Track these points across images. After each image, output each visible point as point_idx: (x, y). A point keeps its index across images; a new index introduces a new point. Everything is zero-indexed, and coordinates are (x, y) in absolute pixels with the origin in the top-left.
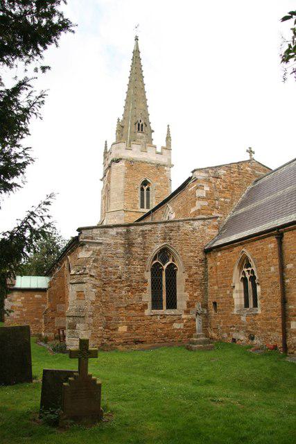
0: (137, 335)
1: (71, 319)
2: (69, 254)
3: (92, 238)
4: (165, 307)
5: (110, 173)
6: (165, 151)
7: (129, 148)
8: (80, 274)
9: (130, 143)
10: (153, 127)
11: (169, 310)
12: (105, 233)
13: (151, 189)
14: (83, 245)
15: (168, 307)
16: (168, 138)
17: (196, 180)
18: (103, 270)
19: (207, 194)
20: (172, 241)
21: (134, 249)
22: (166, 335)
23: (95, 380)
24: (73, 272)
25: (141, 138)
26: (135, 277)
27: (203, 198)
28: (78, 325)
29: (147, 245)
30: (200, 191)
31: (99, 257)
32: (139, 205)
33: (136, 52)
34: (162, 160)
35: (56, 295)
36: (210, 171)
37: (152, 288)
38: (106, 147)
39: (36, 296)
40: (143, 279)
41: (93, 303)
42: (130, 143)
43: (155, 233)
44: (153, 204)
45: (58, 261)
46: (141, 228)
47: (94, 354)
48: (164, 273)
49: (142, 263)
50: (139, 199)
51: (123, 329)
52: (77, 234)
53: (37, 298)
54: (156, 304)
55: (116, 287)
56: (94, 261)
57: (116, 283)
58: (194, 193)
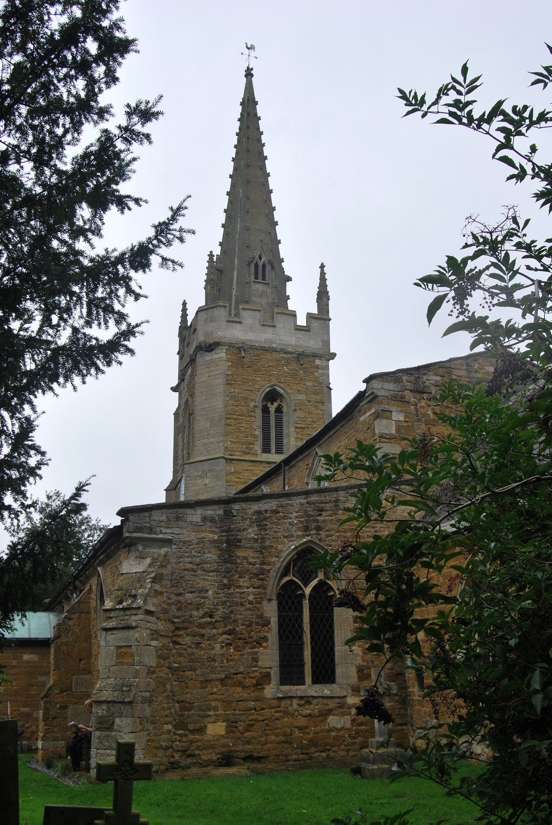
0: (248, 743)
1: (104, 707)
2: (102, 563)
3: (151, 530)
4: (308, 679)
5: (193, 376)
6: (315, 324)
7: (235, 319)
8: (124, 609)
9: (237, 307)
10: (288, 268)
11: (318, 687)
12: (178, 518)
13: (285, 409)
14: (131, 544)
15: (316, 680)
16: (323, 295)
17: (374, 398)
18: (174, 598)
19: (398, 428)
20: (323, 534)
21: (240, 553)
22: (313, 743)
23: (137, 816)
24: (108, 604)
25: (263, 295)
26: (243, 614)
27: (389, 438)
28: (117, 721)
29: (267, 543)
30: (384, 422)
31: (164, 571)
32: (258, 447)
33: (249, 103)
34: (311, 344)
35: (70, 652)
36: (405, 378)
37: (281, 638)
38: (184, 315)
39: (26, 657)
40: (261, 616)
41: (151, 672)
42: (237, 307)
43: (284, 517)
44: (292, 443)
45: (76, 577)
46: (255, 507)
47: (146, 772)
48: (306, 603)
49: (256, 582)
50: (258, 432)
51: (216, 729)
52: (117, 521)
53: (29, 662)
54: (290, 672)
55: (203, 635)
56: (154, 580)
57: (201, 626)
58: (370, 428)
